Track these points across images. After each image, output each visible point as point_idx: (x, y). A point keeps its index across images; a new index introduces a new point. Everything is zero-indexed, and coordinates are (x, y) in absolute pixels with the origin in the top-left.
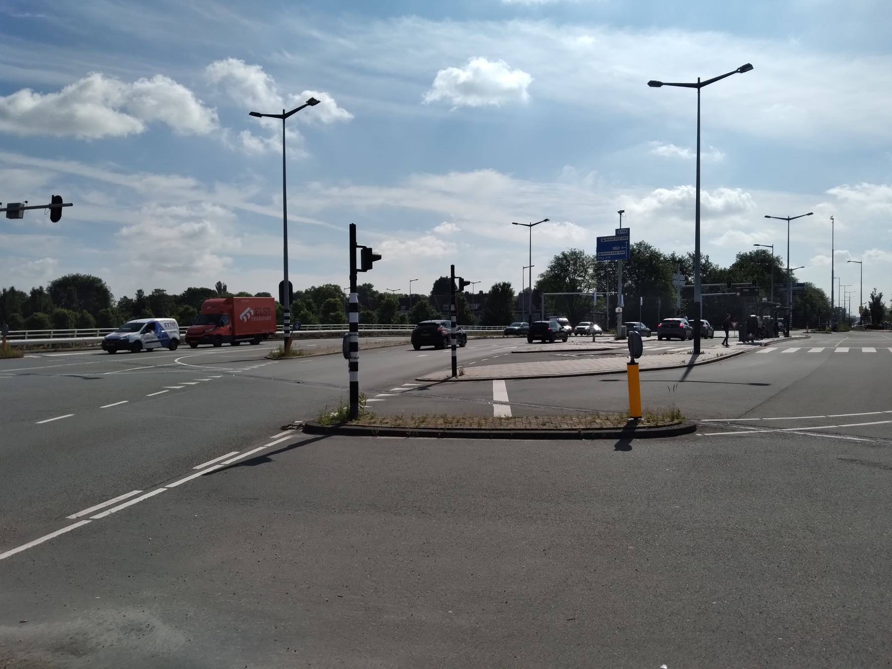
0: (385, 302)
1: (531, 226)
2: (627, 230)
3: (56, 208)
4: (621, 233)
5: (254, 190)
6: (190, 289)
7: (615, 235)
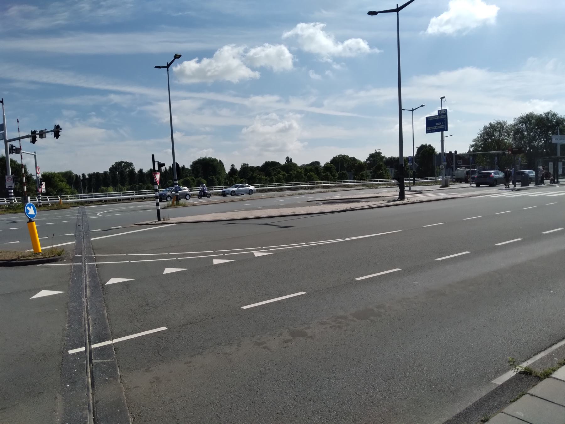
0: (358, 165)
1: (413, 110)
2: (445, 111)
3: (57, 132)
4: (441, 113)
5: (313, 99)
6: (266, 162)
7: (437, 115)
